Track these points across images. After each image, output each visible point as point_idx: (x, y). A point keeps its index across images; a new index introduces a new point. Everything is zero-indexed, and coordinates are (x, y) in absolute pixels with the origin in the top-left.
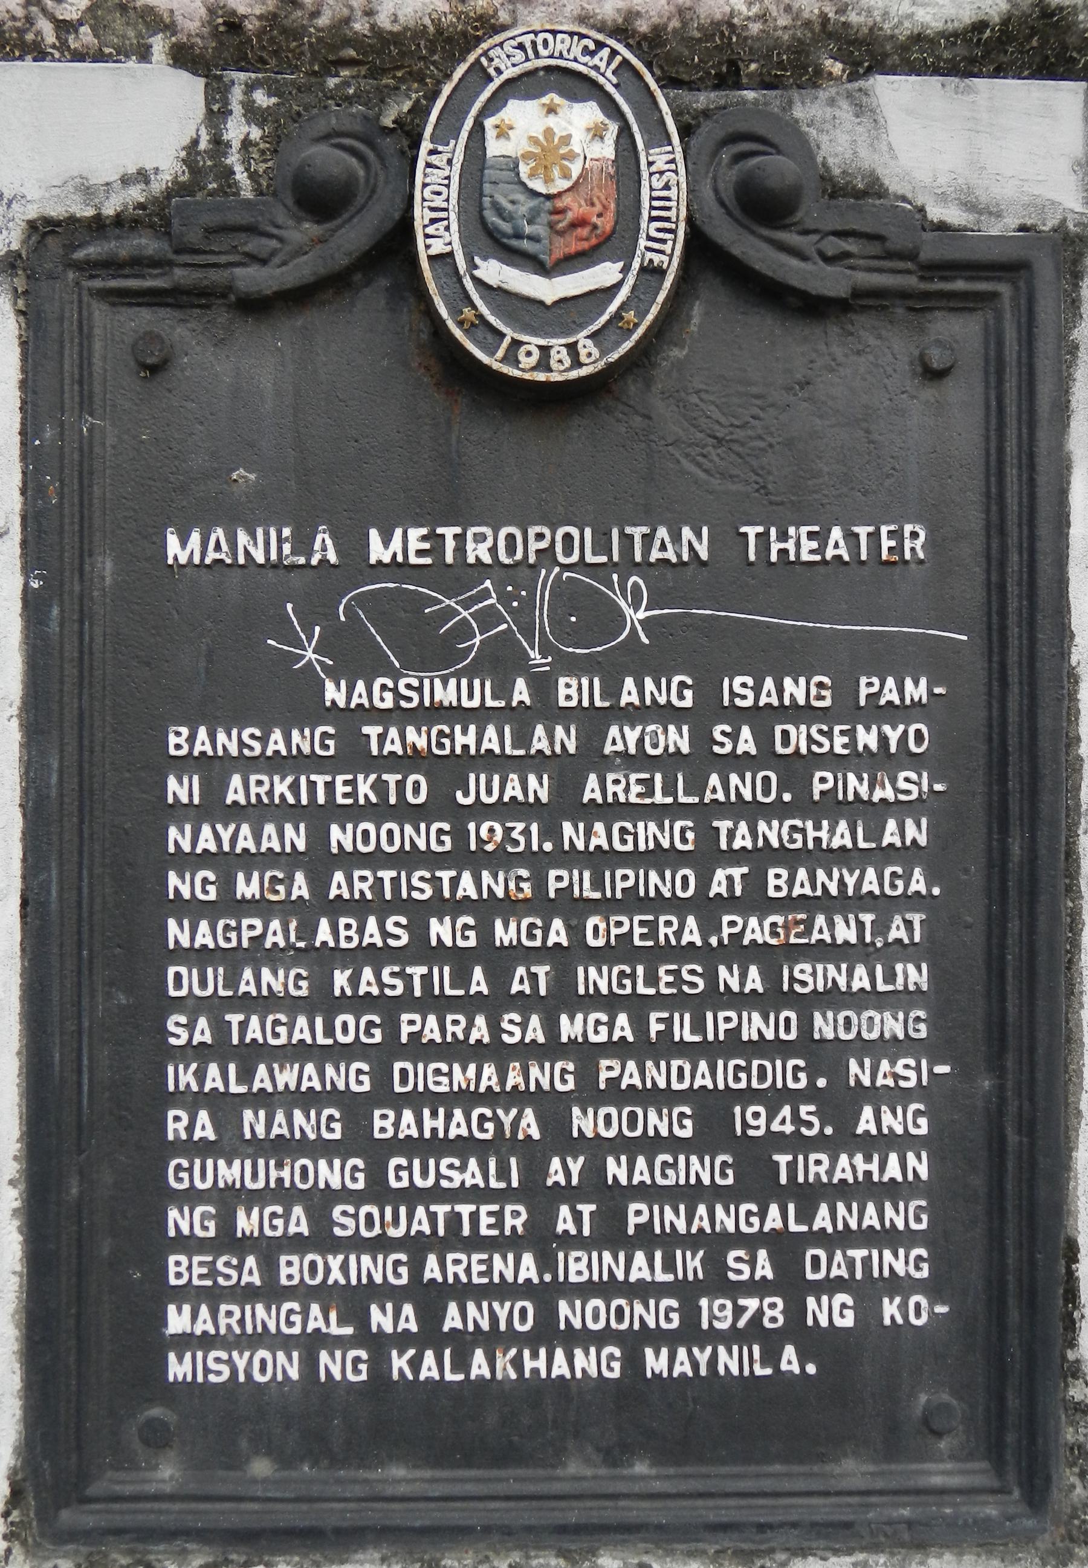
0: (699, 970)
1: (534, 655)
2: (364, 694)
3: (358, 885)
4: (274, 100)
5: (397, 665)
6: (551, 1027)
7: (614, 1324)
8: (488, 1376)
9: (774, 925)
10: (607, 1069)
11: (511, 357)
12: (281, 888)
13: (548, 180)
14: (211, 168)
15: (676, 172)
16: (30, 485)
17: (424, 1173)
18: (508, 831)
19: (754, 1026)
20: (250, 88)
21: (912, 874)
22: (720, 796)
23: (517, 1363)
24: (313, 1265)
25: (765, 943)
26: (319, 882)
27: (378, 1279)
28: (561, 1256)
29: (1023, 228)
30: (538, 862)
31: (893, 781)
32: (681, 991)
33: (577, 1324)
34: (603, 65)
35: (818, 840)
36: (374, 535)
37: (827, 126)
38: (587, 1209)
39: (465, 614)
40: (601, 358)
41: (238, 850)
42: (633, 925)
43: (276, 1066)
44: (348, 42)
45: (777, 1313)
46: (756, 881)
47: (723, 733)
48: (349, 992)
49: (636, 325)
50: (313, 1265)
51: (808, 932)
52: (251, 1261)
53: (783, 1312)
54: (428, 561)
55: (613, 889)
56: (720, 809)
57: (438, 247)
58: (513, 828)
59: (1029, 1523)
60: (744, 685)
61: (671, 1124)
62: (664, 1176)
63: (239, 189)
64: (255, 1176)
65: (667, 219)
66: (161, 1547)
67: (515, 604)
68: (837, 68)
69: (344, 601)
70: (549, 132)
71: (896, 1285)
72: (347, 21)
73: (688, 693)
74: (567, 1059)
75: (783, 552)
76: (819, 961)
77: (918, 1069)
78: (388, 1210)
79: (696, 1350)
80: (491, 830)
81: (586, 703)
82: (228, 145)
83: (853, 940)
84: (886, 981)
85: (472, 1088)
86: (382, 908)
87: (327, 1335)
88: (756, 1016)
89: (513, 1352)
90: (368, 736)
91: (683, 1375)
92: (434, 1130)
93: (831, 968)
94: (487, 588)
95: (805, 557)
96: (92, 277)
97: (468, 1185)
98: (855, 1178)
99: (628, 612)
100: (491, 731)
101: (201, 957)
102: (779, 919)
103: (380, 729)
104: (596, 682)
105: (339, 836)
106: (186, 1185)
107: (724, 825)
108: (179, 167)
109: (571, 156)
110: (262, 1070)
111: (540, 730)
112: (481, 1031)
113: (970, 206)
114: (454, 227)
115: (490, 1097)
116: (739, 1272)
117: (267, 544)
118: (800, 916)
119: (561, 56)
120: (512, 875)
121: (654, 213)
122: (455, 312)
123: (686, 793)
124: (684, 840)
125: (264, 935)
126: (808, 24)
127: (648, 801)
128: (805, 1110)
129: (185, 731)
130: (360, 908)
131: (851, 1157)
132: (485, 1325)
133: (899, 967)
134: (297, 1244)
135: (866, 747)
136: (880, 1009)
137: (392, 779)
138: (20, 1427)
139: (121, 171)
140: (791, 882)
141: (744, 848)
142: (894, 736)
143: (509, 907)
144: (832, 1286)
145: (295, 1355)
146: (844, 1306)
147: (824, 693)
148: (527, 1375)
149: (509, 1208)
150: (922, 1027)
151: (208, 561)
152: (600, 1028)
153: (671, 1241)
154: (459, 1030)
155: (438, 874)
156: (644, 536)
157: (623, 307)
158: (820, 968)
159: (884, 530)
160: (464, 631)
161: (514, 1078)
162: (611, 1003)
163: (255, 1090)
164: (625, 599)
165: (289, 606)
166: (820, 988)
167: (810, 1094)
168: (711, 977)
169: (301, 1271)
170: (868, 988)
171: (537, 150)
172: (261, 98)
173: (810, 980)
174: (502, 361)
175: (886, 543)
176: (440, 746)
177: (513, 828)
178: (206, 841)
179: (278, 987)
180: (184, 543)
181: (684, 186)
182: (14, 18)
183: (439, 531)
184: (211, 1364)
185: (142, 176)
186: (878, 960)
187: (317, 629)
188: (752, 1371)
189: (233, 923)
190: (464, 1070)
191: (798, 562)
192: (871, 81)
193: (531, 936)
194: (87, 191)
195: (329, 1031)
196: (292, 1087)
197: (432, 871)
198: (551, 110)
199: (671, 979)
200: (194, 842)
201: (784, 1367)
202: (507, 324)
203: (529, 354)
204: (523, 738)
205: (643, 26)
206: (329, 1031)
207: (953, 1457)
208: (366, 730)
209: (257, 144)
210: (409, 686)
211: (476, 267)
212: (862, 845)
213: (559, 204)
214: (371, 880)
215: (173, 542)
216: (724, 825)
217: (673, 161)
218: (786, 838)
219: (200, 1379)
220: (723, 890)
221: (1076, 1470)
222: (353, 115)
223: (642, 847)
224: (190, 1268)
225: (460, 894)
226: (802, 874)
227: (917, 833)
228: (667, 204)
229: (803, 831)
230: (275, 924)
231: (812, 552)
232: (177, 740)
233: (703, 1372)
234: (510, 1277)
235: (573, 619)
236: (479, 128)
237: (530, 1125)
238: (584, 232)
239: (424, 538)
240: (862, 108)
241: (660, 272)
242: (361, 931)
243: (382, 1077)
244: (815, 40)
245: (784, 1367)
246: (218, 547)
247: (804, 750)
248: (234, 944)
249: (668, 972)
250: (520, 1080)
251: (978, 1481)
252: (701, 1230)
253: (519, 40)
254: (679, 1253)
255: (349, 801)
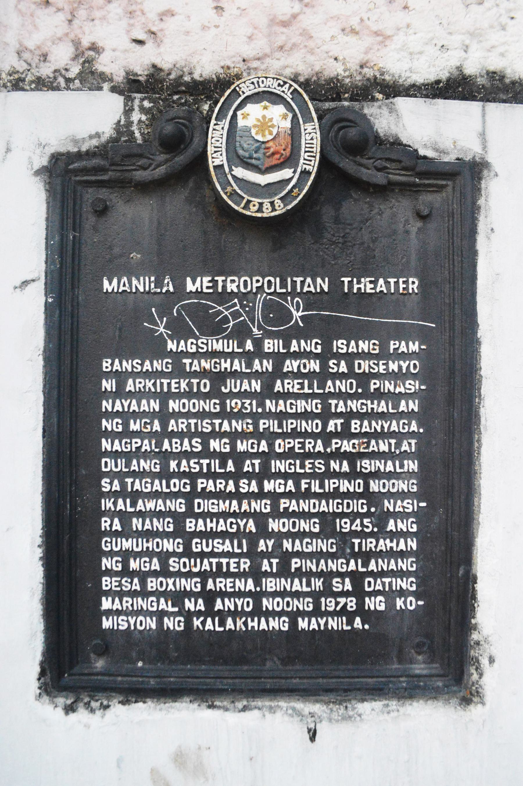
0: (323, 462)
1: (255, 330)
2: (184, 346)
3: (180, 426)
4: (152, 104)
5: (198, 334)
6: (260, 486)
7: (285, 608)
8: (233, 628)
9: (354, 444)
10: (284, 503)
11: (246, 207)
12: (148, 426)
13: (264, 135)
14: (125, 132)
15: (316, 133)
16: (49, 260)
17: (207, 546)
18: (243, 404)
19: (345, 486)
20: (142, 100)
21: (411, 424)
22: (332, 390)
23: (245, 623)
24: (161, 583)
25: (350, 452)
26: (164, 425)
27: (188, 589)
28: (264, 580)
29: (458, 159)
30: (255, 417)
31: (404, 385)
32: (314, 471)
33: (270, 608)
34: (286, 91)
35: (372, 409)
36: (189, 280)
37: (377, 117)
38: (275, 561)
39: (226, 313)
40: (284, 207)
41: (131, 411)
42: (295, 443)
43: (146, 500)
44: (181, 84)
45: (353, 604)
46: (346, 426)
47: (334, 364)
48: (176, 470)
49: (299, 195)
50: (161, 583)
51: (368, 447)
52: (136, 580)
53: (356, 604)
54: (211, 291)
55: (287, 428)
56: (331, 395)
57: (217, 162)
58: (245, 403)
59: (455, 688)
60: (342, 344)
61: (310, 527)
62: (307, 547)
63: (136, 140)
64: (137, 545)
65: (312, 152)
66: (100, 694)
67: (247, 309)
68: (380, 96)
69: (176, 307)
70: (264, 117)
71: (402, 593)
72: (181, 76)
73: (319, 347)
74: (268, 499)
75: (359, 289)
76: (372, 459)
77: (413, 504)
78: (192, 560)
79: (319, 619)
80: (236, 403)
81: (276, 351)
82: (132, 122)
83: (387, 451)
84: (400, 468)
85: (227, 511)
86: (191, 435)
87: (167, 611)
88: (346, 482)
89: (244, 619)
90: (185, 364)
91: (314, 630)
92: (212, 528)
93: (377, 462)
94: (235, 303)
95: (368, 291)
96: (76, 176)
97: (225, 551)
98: (386, 549)
99: (294, 312)
100: (236, 362)
101: (116, 455)
102: (356, 441)
103: (190, 361)
104: (281, 341)
105: (173, 405)
106: (109, 549)
107: (333, 402)
108: (112, 132)
109: (273, 126)
110: (140, 502)
111: (257, 362)
112: (231, 487)
113: (436, 150)
114: (224, 154)
115: (234, 515)
116: (337, 587)
117: (144, 283)
118: (365, 440)
119: (269, 87)
120: (245, 422)
121: (307, 149)
122: (223, 189)
123: (318, 388)
124: (317, 408)
125: (141, 446)
126: (368, 79)
127: (302, 392)
128: (366, 521)
129: (110, 361)
130: (181, 435)
131: (385, 540)
132: (232, 608)
133: (406, 462)
134: (155, 574)
135: (393, 370)
136: (398, 479)
137: (195, 381)
138: (43, 645)
139: (89, 133)
140: (361, 426)
141: (342, 412)
142: (404, 365)
143: (244, 435)
144: (376, 593)
145: (154, 619)
146: (381, 601)
147: (375, 347)
148: (250, 628)
149: (242, 560)
150: (415, 487)
151: (120, 291)
152: (281, 486)
153: (309, 574)
154: (222, 487)
155: (214, 421)
156: (301, 281)
157: (294, 187)
158: (373, 462)
159: (401, 280)
160: (226, 320)
161: (245, 506)
162: (286, 476)
163: (137, 510)
164: (293, 307)
165: (153, 309)
166: (373, 471)
167: (368, 514)
168: (327, 465)
169: (157, 585)
170: (393, 471)
171: (259, 124)
172: (147, 104)
173: (369, 467)
174: (244, 208)
175: (402, 286)
176: (215, 368)
177: (245, 403)
178: (118, 407)
179: (147, 468)
180: (110, 284)
181: (319, 139)
182: (49, 78)
183: (216, 278)
184: (120, 622)
185: (98, 135)
186: (397, 459)
187: (165, 319)
188: (342, 628)
189: (129, 441)
190: (224, 503)
191: (365, 293)
192: (396, 99)
193: (252, 448)
194: (75, 141)
195: (168, 486)
196: (153, 509)
197: (211, 420)
198: (265, 108)
199: (311, 466)
200: (113, 407)
201: (355, 626)
202: (245, 193)
203: (254, 205)
204: (249, 365)
205: (302, 79)
206: (168, 486)
207: (424, 662)
208: (184, 361)
209: (144, 122)
210: (202, 343)
211: (233, 170)
212: (391, 411)
213: (268, 145)
214: (186, 424)
215: (106, 283)
216: (333, 402)
217: (315, 129)
218: (359, 408)
219: (116, 628)
220: (333, 429)
221: (474, 667)
222: (183, 110)
223: (299, 411)
224: (111, 583)
225: (223, 430)
226: (366, 423)
227: (414, 406)
228: (312, 146)
229: (366, 405)
230: (146, 442)
231: (371, 289)
232: (106, 365)
233: (322, 628)
234: (243, 589)
235: (271, 315)
236: (234, 116)
237: (251, 526)
238: (277, 156)
239: (210, 282)
240: (392, 110)
241: (309, 173)
242: (181, 445)
243: (190, 505)
244: (371, 86)
245: (355, 626)
246: (124, 285)
247: (367, 371)
248: (129, 450)
249: (309, 463)
250: (248, 507)
251: (434, 672)
252: (322, 570)
253: (252, 80)
254: (313, 579)
255: (177, 391)
